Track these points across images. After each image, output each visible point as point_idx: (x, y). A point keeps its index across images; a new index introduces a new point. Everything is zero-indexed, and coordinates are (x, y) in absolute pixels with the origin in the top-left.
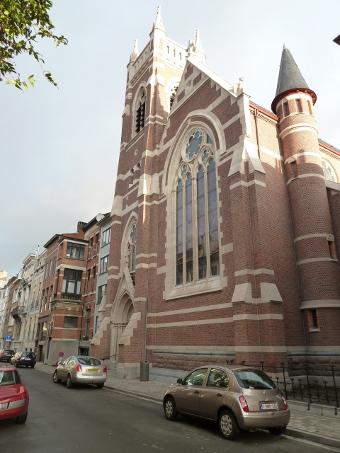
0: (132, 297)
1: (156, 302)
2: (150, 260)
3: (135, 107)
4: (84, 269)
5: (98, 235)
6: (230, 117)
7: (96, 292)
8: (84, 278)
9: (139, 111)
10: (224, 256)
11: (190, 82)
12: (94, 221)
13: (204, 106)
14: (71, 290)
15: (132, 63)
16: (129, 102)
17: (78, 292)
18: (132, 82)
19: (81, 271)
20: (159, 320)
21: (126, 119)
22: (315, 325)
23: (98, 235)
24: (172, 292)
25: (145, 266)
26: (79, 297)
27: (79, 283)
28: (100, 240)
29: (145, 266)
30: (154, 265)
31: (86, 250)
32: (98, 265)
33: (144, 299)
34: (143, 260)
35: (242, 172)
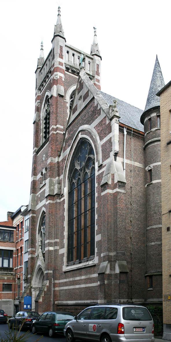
0: (43, 269)
1: (57, 273)
2: (56, 244)
3: (43, 114)
4: (14, 249)
5: (22, 223)
6: (106, 135)
7: (23, 266)
8: (14, 256)
9: (46, 119)
10: (98, 242)
11: (81, 97)
12: (19, 212)
13: (89, 122)
14: (6, 265)
15: (39, 70)
16: (38, 109)
17: (11, 266)
18: (40, 89)
19: (12, 251)
20: (65, 284)
21: (36, 123)
22: (151, 286)
23: (22, 223)
24: (65, 268)
25: (51, 248)
26: (11, 270)
27: (11, 260)
28: (81, 65)
29: (51, 248)
30: (57, 248)
31: (15, 234)
32: (24, 246)
33: (51, 272)
34: (50, 245)
35: (110, 182)
